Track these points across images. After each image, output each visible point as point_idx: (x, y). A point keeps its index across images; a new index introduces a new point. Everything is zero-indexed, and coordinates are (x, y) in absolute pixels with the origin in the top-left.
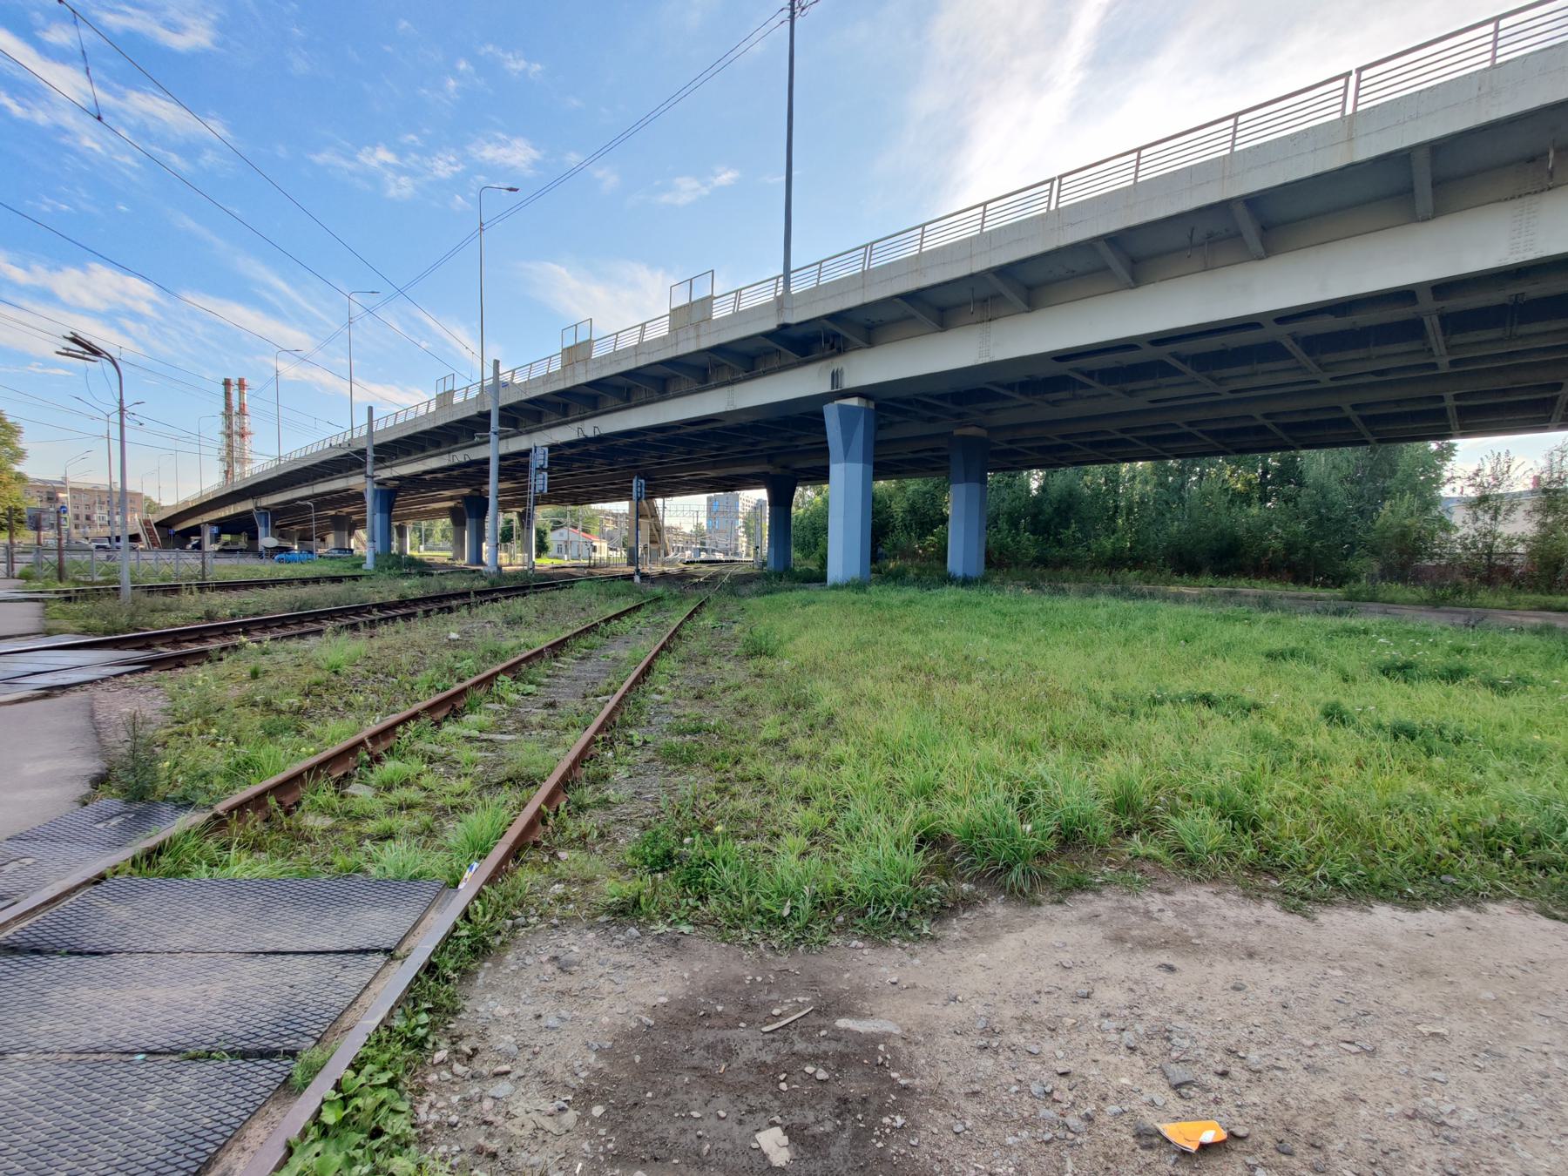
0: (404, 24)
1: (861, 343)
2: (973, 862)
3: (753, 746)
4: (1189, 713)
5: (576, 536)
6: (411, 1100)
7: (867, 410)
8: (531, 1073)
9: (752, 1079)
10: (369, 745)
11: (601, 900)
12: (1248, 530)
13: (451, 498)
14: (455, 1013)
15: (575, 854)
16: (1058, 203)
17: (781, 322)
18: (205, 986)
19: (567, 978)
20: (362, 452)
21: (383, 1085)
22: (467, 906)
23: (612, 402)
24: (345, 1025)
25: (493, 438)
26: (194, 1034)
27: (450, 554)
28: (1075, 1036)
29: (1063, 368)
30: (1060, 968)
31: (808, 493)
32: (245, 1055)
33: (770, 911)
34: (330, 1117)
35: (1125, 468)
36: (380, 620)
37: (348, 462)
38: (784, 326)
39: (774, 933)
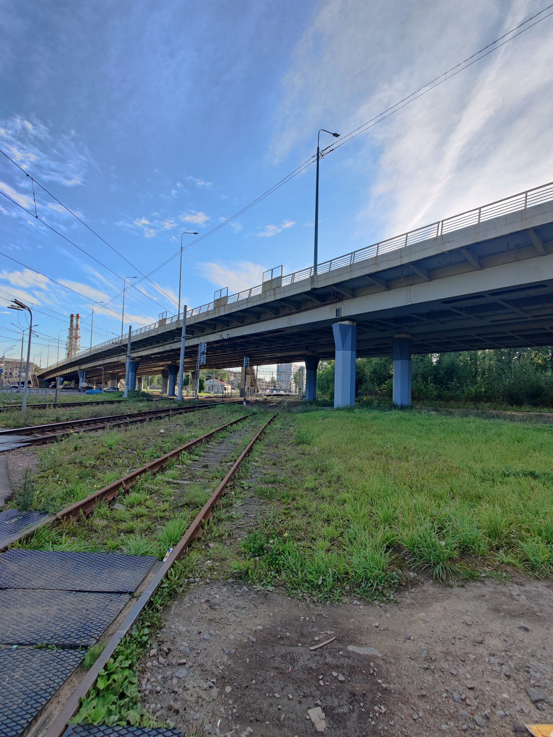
0: (156, 170)
1: (350, 296)
2: (415, 560)
3: (301, 492)
4: (524, 481)
5: (217, 382)
6: (139, 676)
7: (353, 326)
8: (196, 665)
9: (305, 677)
10: (124, 485)
11: (230, 570)
12: (546, 384)
13: (163, 366)
14: (160, 628)
15: (217, 545)
16: (442, 232)
17: (313, 287)
18: (47, 608)
19: (213, 612)
20: (126, 346)
21: (126, 668)
22: (167, 571)
23: (235, 323)
24: (110, 633)
25: (183, 339)
26: (41, 634)
27: (161, 391)
28: (476, 666)
29: (447, 307)
30: (465, 625)
31: (324, 363)
32: (63, 647)
33: (312, 581)
34: (101, 685)
35: (480, 352)
36: (130, 422)
37: (119, 349)
38: (314, 289)
39: (314, 593)
